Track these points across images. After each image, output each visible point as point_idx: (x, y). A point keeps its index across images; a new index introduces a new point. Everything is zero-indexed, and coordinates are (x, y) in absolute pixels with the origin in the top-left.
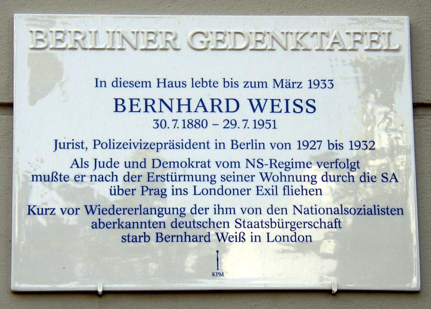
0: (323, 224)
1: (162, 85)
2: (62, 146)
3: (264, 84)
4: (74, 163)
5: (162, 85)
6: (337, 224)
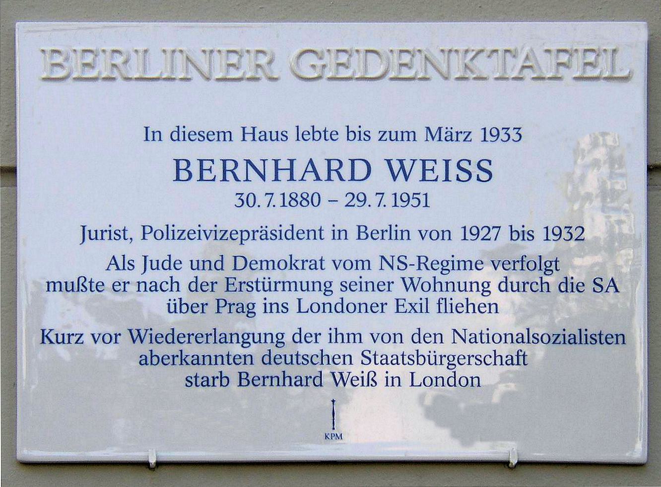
0: (498, 359)
1: (249, 137)
2: (93, 236)
3: (411, 135)
4: (610, 285)
5: (249, 137)
6: (521, 358)
